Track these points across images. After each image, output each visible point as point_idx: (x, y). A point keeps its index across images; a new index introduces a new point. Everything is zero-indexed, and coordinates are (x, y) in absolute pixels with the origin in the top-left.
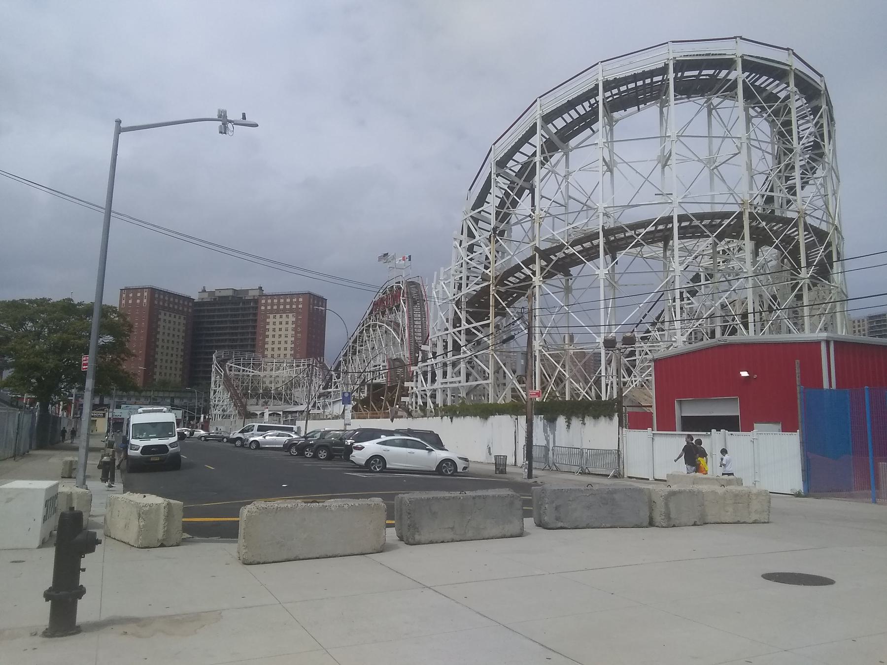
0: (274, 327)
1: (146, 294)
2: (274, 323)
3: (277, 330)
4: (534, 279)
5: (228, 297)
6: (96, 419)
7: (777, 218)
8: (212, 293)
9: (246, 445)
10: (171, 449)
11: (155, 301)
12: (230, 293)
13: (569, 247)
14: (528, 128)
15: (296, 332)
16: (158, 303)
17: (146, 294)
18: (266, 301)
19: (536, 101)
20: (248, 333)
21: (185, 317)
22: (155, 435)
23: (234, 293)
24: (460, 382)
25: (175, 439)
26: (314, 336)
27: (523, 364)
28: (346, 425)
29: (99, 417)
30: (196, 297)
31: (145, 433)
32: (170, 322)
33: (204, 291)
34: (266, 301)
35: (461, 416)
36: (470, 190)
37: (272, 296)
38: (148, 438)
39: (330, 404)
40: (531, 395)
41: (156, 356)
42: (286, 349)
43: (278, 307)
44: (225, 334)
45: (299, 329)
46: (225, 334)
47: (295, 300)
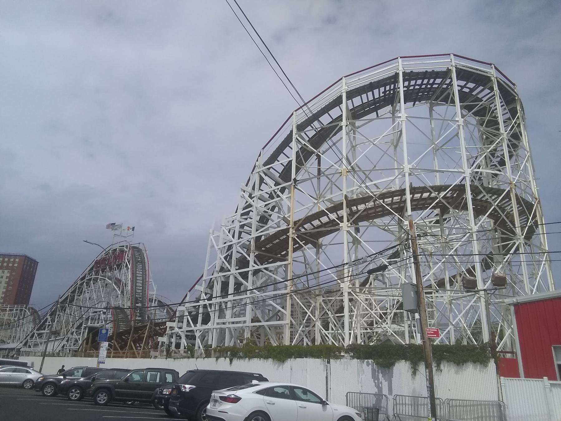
4: (341, 225)
7: (525, 201)
14: (332, 100)
19: (342, 79)
24: (245, 322)
26: (23, 290)
27: (413, 296)
28: (99, 363)
35: (246, 357)
36: (263, 149)
39: (41, 344)
40: (428, 334)
47: (12, 260)
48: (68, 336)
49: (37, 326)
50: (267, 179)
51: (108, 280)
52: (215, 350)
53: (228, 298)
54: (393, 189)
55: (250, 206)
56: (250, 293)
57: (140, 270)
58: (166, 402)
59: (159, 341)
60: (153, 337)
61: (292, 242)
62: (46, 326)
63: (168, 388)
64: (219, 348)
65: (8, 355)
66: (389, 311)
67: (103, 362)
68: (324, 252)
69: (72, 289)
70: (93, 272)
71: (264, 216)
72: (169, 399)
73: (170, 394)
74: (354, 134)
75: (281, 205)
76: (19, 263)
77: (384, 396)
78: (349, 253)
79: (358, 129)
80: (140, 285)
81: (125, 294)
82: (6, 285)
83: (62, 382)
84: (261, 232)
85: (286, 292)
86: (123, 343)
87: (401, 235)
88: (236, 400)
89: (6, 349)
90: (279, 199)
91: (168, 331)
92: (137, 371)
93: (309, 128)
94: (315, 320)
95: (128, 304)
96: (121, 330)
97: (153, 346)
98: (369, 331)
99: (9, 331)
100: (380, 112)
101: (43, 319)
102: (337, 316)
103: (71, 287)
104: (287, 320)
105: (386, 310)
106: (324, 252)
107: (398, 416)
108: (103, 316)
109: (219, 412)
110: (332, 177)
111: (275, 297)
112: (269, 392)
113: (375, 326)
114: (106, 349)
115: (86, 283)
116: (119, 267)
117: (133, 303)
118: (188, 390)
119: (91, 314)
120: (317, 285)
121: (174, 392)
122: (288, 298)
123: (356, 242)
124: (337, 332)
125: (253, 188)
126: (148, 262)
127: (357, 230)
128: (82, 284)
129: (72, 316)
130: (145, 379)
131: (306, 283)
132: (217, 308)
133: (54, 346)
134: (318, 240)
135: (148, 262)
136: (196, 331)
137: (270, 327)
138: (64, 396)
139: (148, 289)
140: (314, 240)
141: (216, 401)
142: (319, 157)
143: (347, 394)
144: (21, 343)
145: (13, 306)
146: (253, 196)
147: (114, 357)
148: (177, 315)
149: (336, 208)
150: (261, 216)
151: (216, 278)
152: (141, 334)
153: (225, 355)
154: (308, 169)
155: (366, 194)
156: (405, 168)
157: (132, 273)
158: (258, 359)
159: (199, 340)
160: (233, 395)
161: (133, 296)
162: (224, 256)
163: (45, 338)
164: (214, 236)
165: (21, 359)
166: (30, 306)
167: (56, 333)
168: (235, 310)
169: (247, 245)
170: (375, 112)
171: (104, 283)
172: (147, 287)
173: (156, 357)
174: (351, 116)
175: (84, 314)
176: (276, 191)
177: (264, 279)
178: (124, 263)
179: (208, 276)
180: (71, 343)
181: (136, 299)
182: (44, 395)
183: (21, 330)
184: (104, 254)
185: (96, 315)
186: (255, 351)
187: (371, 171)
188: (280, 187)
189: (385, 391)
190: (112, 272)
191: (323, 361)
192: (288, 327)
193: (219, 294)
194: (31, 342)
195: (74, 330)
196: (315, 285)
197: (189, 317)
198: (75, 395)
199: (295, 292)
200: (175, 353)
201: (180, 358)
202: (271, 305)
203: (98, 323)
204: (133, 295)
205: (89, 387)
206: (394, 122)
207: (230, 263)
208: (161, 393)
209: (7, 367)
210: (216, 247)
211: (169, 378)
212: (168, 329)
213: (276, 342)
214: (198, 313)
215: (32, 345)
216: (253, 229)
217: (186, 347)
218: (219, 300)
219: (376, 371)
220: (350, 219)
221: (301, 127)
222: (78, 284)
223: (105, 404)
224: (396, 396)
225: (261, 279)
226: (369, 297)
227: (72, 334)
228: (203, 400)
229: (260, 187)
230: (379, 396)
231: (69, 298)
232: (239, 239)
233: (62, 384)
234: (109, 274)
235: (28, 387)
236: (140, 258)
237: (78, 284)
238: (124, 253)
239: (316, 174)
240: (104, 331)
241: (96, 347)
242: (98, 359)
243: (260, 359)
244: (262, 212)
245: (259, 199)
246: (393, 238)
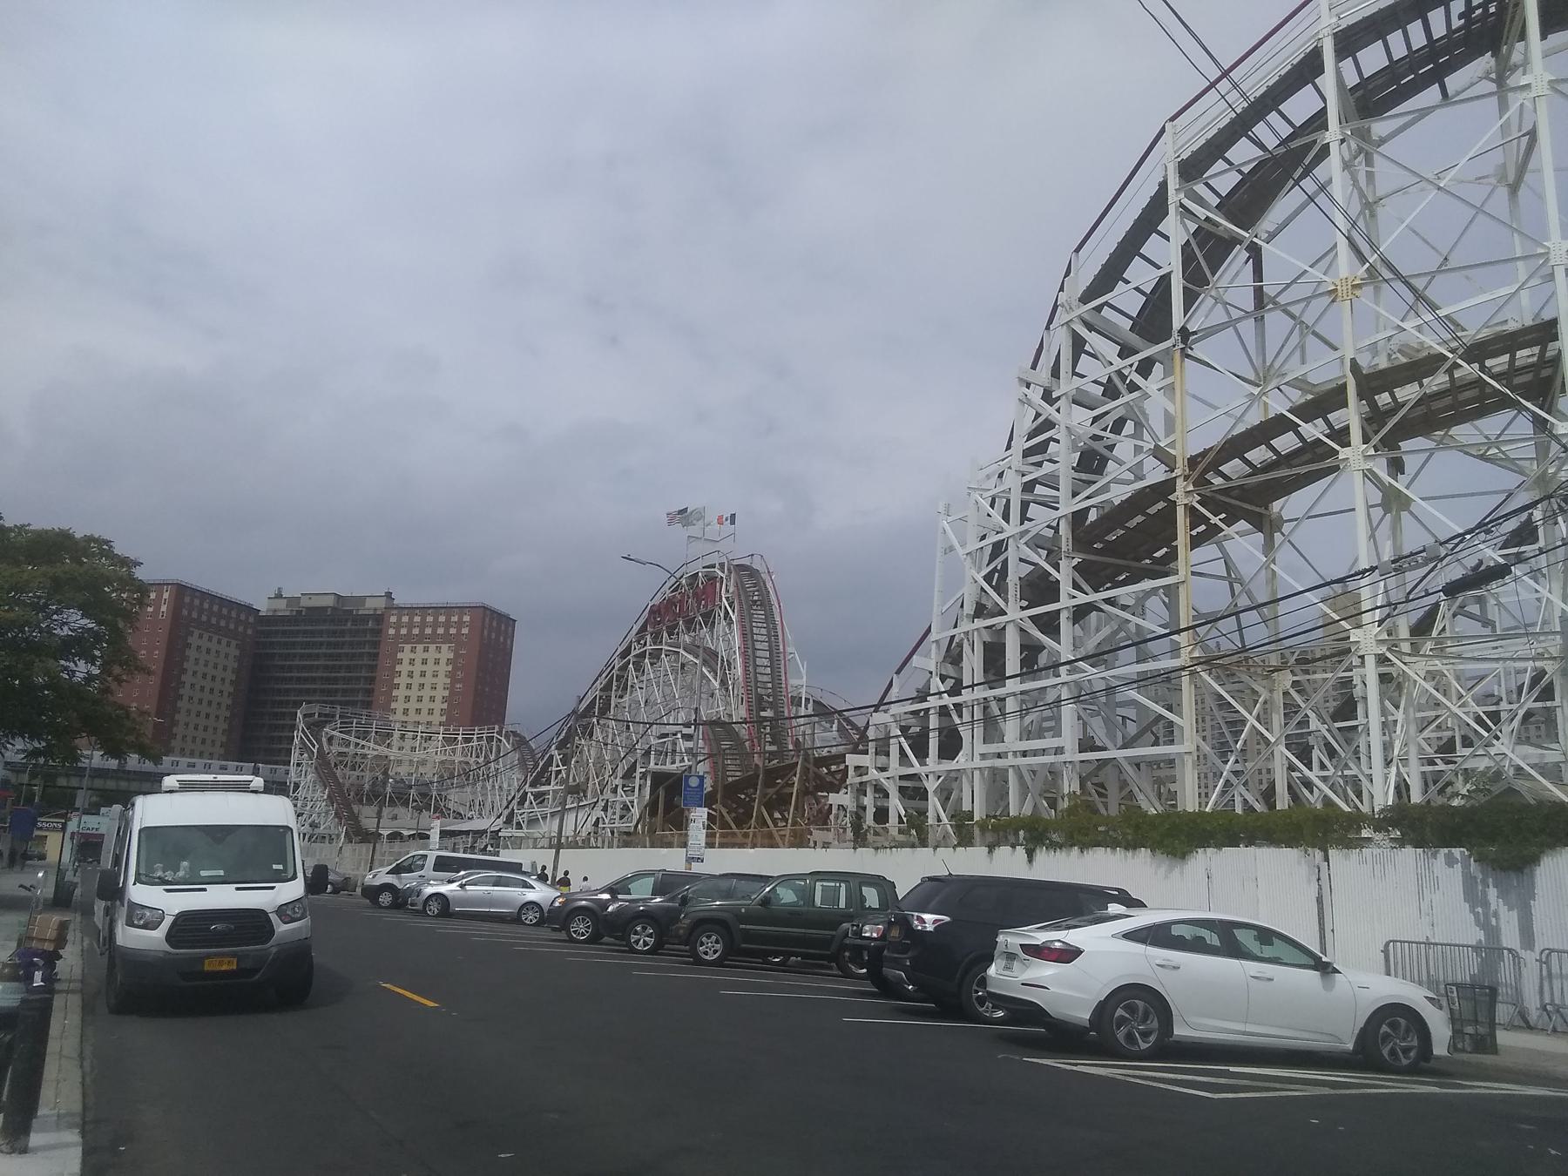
0: (411, 668)
1: (166, 595)
2: (412, 662)
3: (417, 674)
4: (1344, 453)
5: (324, 609)
6: (47, 833)
9: (412, 905)
10: (281, 928)
11: (184, 610)
12: (329, 602)
13: (1459, 361)
14: (1289, 67)
15: (454, 681)
16: (190, 614)
17: (166, 595)
18: (399, 619)
20: (358, 679)
21: (239, 642)
22: (221, 873)
23: (338, 602)
24: (1059, 751)
25: (292, 890)
28: (690, 860)
29: (54, 829)
30: (263, 605)
31: (185, 864)
32: (208, 651)
33: (279, 596)
34: (399, 619)
35: (1072, 846)
36: (1077, 250)
37: (411, 610)
38: (195, 882)
39: (544, 818)
41: (177, 717)
42: (227, 656)
44: (314, 680)
45: (460, 674)
46: (314, 680)
47: (455, 619)
48: (605, 797)
49: (531, 776)
50: (1094, 340)
51: (686, 654)
52: (983, 826)
53: (1005, 686)
54: (1512, 326)
55: (1049, 425)
56: (1070, 672)
57: (760, 625)
58: (874, 957)
59: (831, 805)
60: (813, 794)
61: (1185, 518)
62: (551, 774)
63: (877, 921)
64: (993, 820)
65: (473, 847)
66: (1504, 705)
67: (699, 858)
68: (1289, 541)
69: (603, 681)
70: (648, 637)
71: (1093, 450)
72: (880, 950)
73: (883, 937)
74: (1369, 162)
75: (1144, 414)
76: (471, 626)
77: (1505, 951)
78: (1372, 537)
79: (1379, 146)
80: (766, 662)
81: (730, 688)
82: (449, 681)
83: (610, 909)
84: (1088, 498)
85: (1176, 663)
86: (741, 811)
87: (1547, 469)
88: (1068, 955)
89: (467, 833)
90: (1136, 394)
91: (852, 779)
92: (787, 879)
93: (1220, 165)
94: (1273, 740)
95: (740, 713)
96: (730, 779)
97: (814, 817)
98: (1441, 766)
99: (469, 789)
100: (1454, 81)
101: (543, 759)
102: (1338, 728)
103: (600, 675)
104: (1188, 743)
105: (1497, 704)
106: (1289, 541)
107: (1558, 1011)
108: (683, 745)
109: (1023, 984)
110: (1303, 311)
111: (1142, 681)
112: (1157, 936)
113: (1461, 751)
114: (704, 825)
116: (709, 619)
117: (752, 710)
118: (930, 928)
119: (654, 741)
120: (1272, 639)
121: (895, 933)
122: (1185, 680)
123: (1394, 502)
124: (1342, 772)
125: (1055, 372)
126: (779, 604)
127: (1397, 467)
128: (624, 668)
129: (609, 747)
130: (811, 899)
131: (1236, 637)
132: (978, 714)
133: (576, 820)
134: (1267, 509)
135: (779, 604)
136: (927, 776)
137: (1137, 764)
138: (617, 942)
139: (786, 673)
140: (1258, 509)
141: (1011, 957)
142: (1255, 253)
143: (1387, 945)
144: (499, 817)
145: (471, 730)
146: (1054, 395)
147: (722, 846)
148: (871, 734)
149: (1324, 402)
150: (1082, 453)
151: (967, 633)
152: (783, 787)
153: (1012, 839)
154: (1222, 293)
155: (1418, 351)
156: (1552, 253)
157: (743, 634)
158: (1108, 849)
159: (936, 799)
160: (1059, 941)
161: (750, 692)
162: (984, 573)
163: (552, 805)
164: (950, 519)
165: (506, 856)
166: (508, 728)
167: (577, 790)
168: (1028, 719)
169: (1050, 538)
170: (1437, 85)
171: (676, 661)
172: (782, 666)
173: (826, 845)
174: (1354, 108)
175: (638, 742)
176: (1126, 372)
177: (1106, 631)
178: (720, 608)
179: (943, 630)
180: (614, 813)
181: (760, 698)
182: (572, 940)
183: (494, 786)
185: (665, 742)
186: (1096, 827)
187: (1432, 275)
188: (1135, 359)
189: (1510, 937)
190: (693, 634)
191: (1306, 853)
192: (1189, 761)
193: (979, 678)
194: (521, 815)
195: (618, 781)
196: (1266, 641)
197: (902, 739)
199: (1208, 662)
200: (876, 834)
201: (891, 848)
202: (1134, 703)
203: (673, 763)
204: (749, 688)
205: (678, 920)
206: (1503, 106)
207: (1001, 589)
208: (858, 934)
209: (479, 873)
210: (961, 552)
211: (872, 897)
212: (851, 772)
213: (1157, 805)
214: (925, 731)
216: (1064, 493)
217: (905, 819)
218: (981, 693)
219: (1479, 881)
220: (1370, 433)
221: (1192, 169)
222: (616, 668)
223: (717, 963)
224: (1550, 953)
225: (1098, 630)
226: (1438, 664)
227: (615, 791)
228: (971, 956)
229: (1074, 366)
230: (1491, 951)
231: (597, 704)
232: (1022, 523)
233: (611, 913)
234: (687, 638)
235: (531, 921)
236: (756, 593)
237: (616, 668)
238: (718, 584)
239: (1250, 307)
240: (694, 782)
241: (679, 822)
242: (687, 851)
243: (1114, 848)
244: (1086, 438)
245: (1075, 402)
246: (1510, 480)
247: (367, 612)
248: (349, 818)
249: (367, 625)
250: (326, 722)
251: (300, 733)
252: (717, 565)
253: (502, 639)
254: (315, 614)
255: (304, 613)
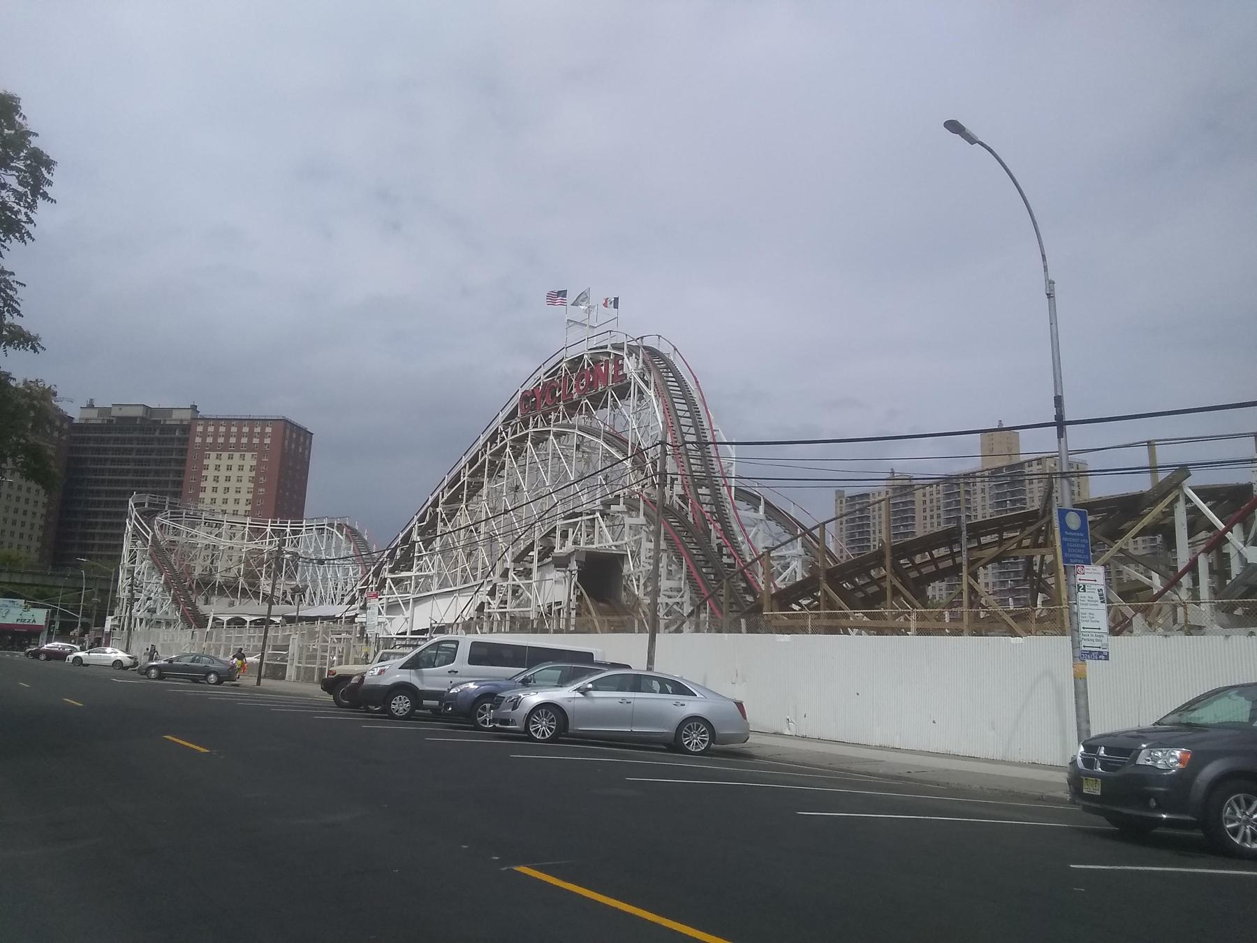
0: (216, 473)
2: (217, 468)
3: (222, 479)
5: (135, 418)
8: (104, 411)
12: (138, 412)
18: (205, 429)
33: (91, 406)
37: (217, 421)
39: (406, 603)
43: (215, 439)
47: (258, 430)
67: (1101, 653)
76: (272, 436)
115: (553, 435)
130: (672, 682)
184: (544, 374)
195: (509, 564)
198: (43, 657)
215: (383, 607)
227: (505, 575)
247: (172, 423)
248: (186, 604)
249: (175, 434)
250: (157, 512)
251: (133, 521)
252: (609, 346)
253: (300, 450)
254: (126, 423)
255: (114, 422)
